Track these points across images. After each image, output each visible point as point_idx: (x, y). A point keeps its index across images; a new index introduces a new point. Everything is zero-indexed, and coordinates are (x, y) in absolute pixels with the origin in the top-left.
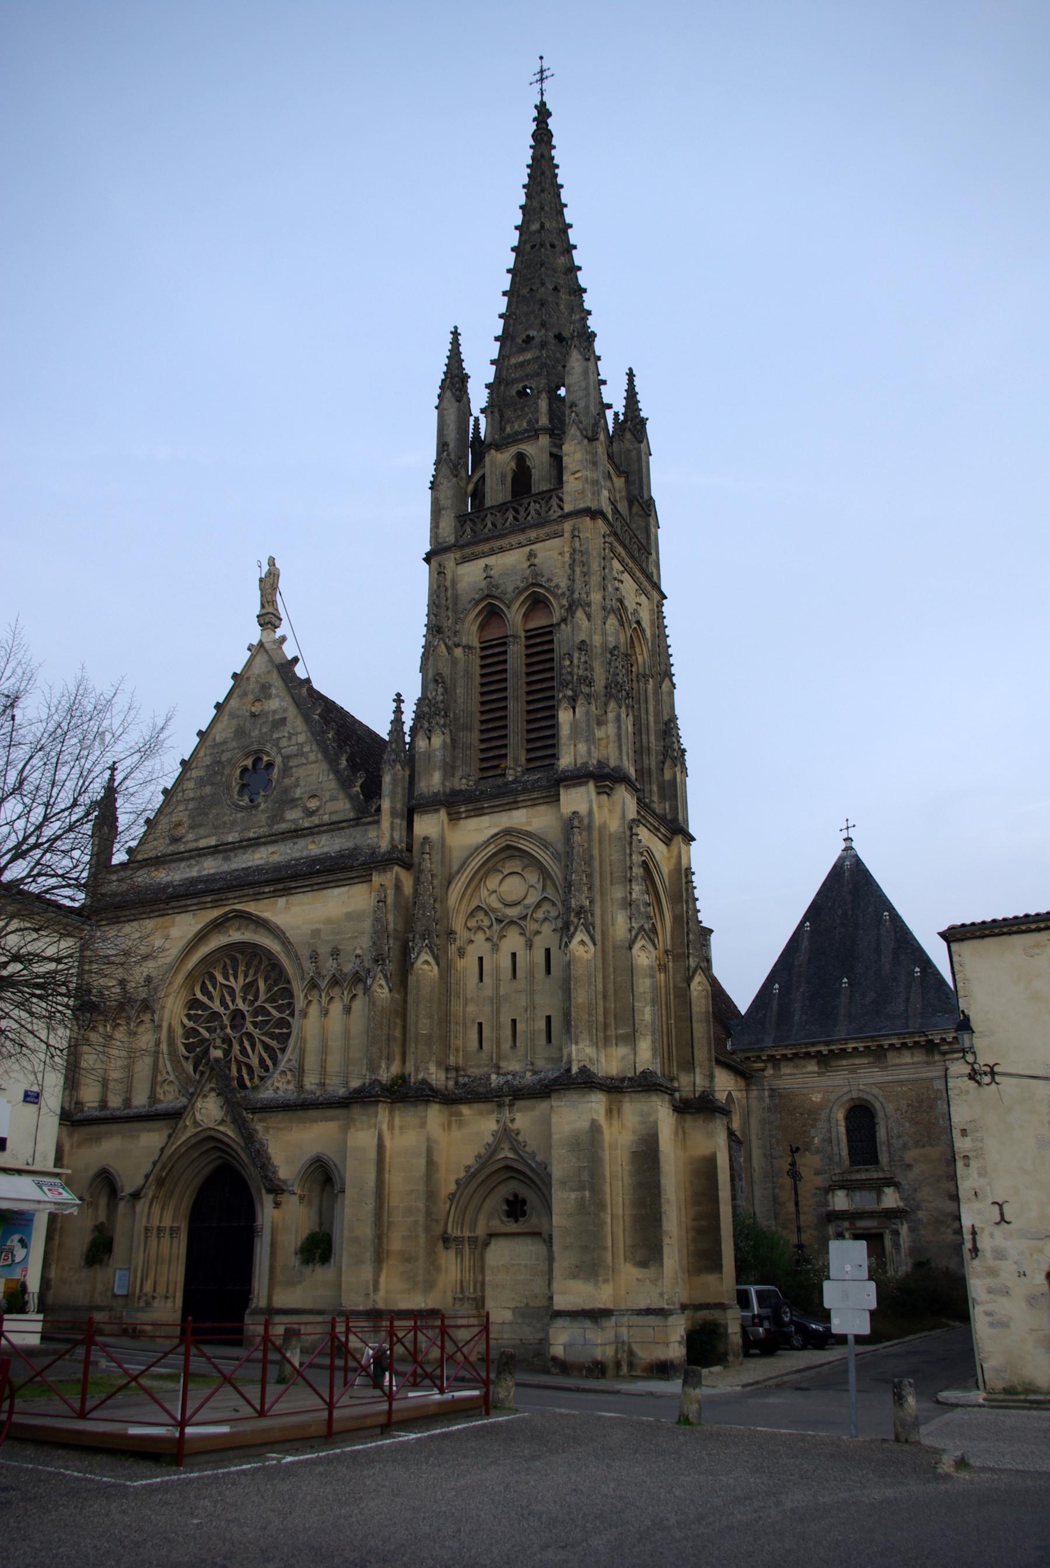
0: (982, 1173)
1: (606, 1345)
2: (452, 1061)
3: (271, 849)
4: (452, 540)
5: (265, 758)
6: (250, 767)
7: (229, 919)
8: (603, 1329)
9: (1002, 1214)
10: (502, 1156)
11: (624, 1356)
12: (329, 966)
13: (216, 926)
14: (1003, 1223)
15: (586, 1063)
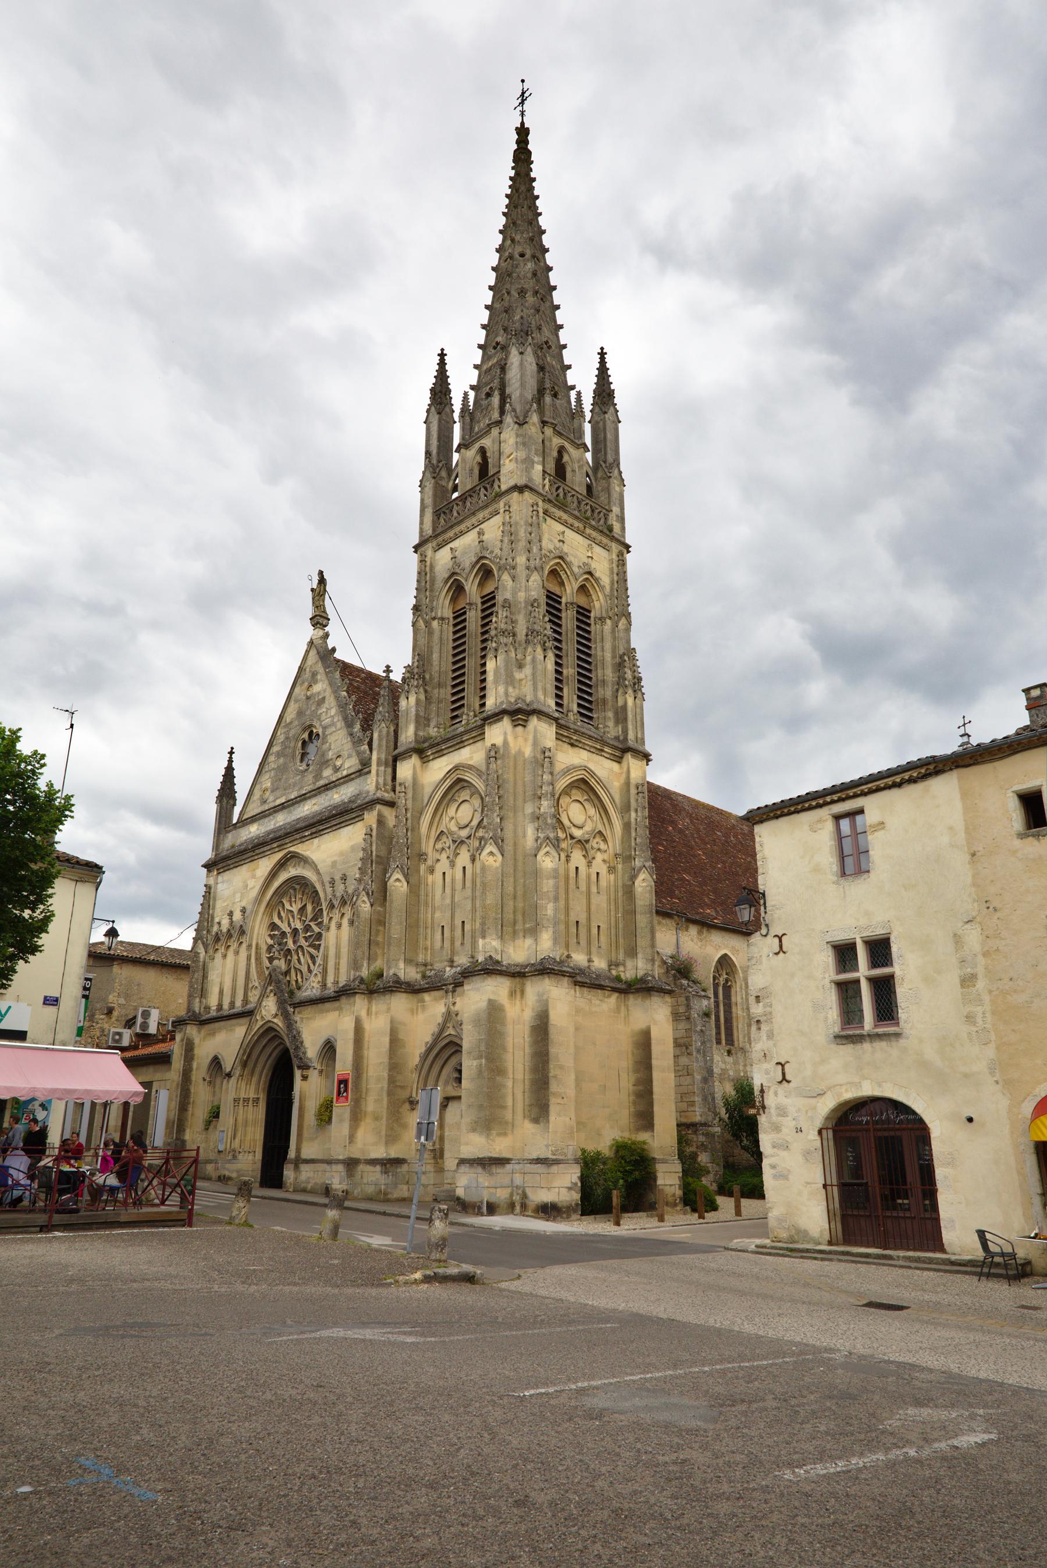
0: (770, 1036)
1: (496, 1188)
2: (421, 958)
3: (314, 801)
4: (430, 532)
5: (315, 731)
6: (307, 739)
7: (288, 860)
8: (491, 1174)
9: (784, 1074)
10: (448, 1033)
11: (517, 1198)
12: (340, 888)
13: (281, 865)
14: (784, 1082)
15: (492, 954)
